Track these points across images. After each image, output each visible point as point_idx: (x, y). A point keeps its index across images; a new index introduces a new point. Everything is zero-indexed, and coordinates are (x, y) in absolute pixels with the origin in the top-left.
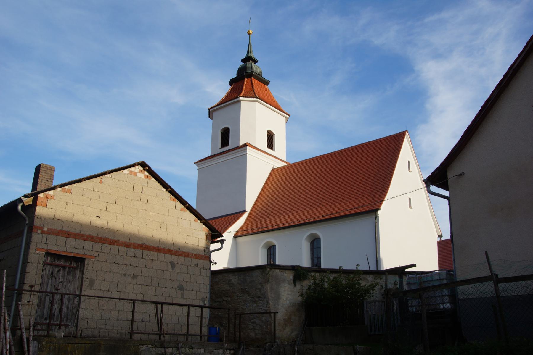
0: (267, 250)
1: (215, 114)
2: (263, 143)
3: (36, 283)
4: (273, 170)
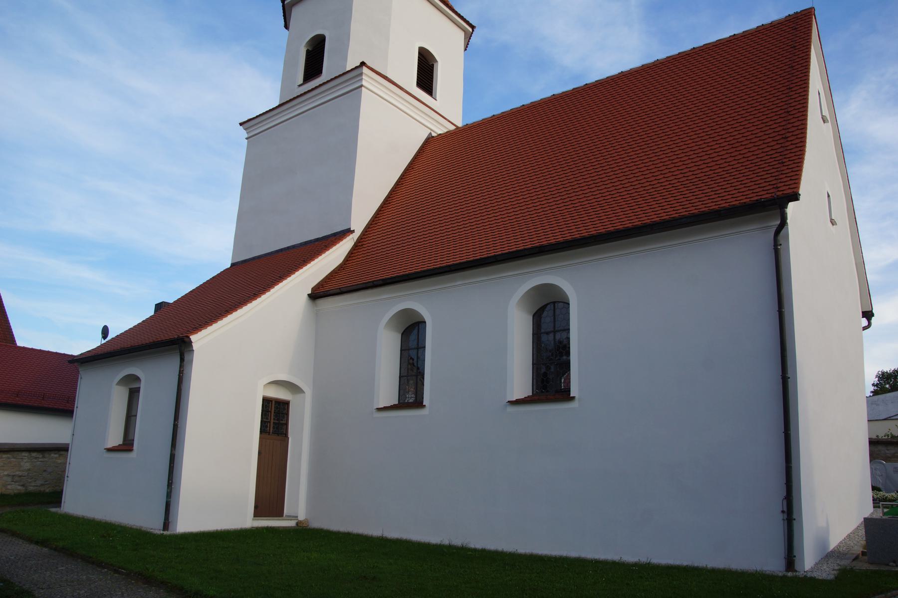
0: (400, 336)
2: (409, 75)
3: (416, 351)
4: (429, 140)
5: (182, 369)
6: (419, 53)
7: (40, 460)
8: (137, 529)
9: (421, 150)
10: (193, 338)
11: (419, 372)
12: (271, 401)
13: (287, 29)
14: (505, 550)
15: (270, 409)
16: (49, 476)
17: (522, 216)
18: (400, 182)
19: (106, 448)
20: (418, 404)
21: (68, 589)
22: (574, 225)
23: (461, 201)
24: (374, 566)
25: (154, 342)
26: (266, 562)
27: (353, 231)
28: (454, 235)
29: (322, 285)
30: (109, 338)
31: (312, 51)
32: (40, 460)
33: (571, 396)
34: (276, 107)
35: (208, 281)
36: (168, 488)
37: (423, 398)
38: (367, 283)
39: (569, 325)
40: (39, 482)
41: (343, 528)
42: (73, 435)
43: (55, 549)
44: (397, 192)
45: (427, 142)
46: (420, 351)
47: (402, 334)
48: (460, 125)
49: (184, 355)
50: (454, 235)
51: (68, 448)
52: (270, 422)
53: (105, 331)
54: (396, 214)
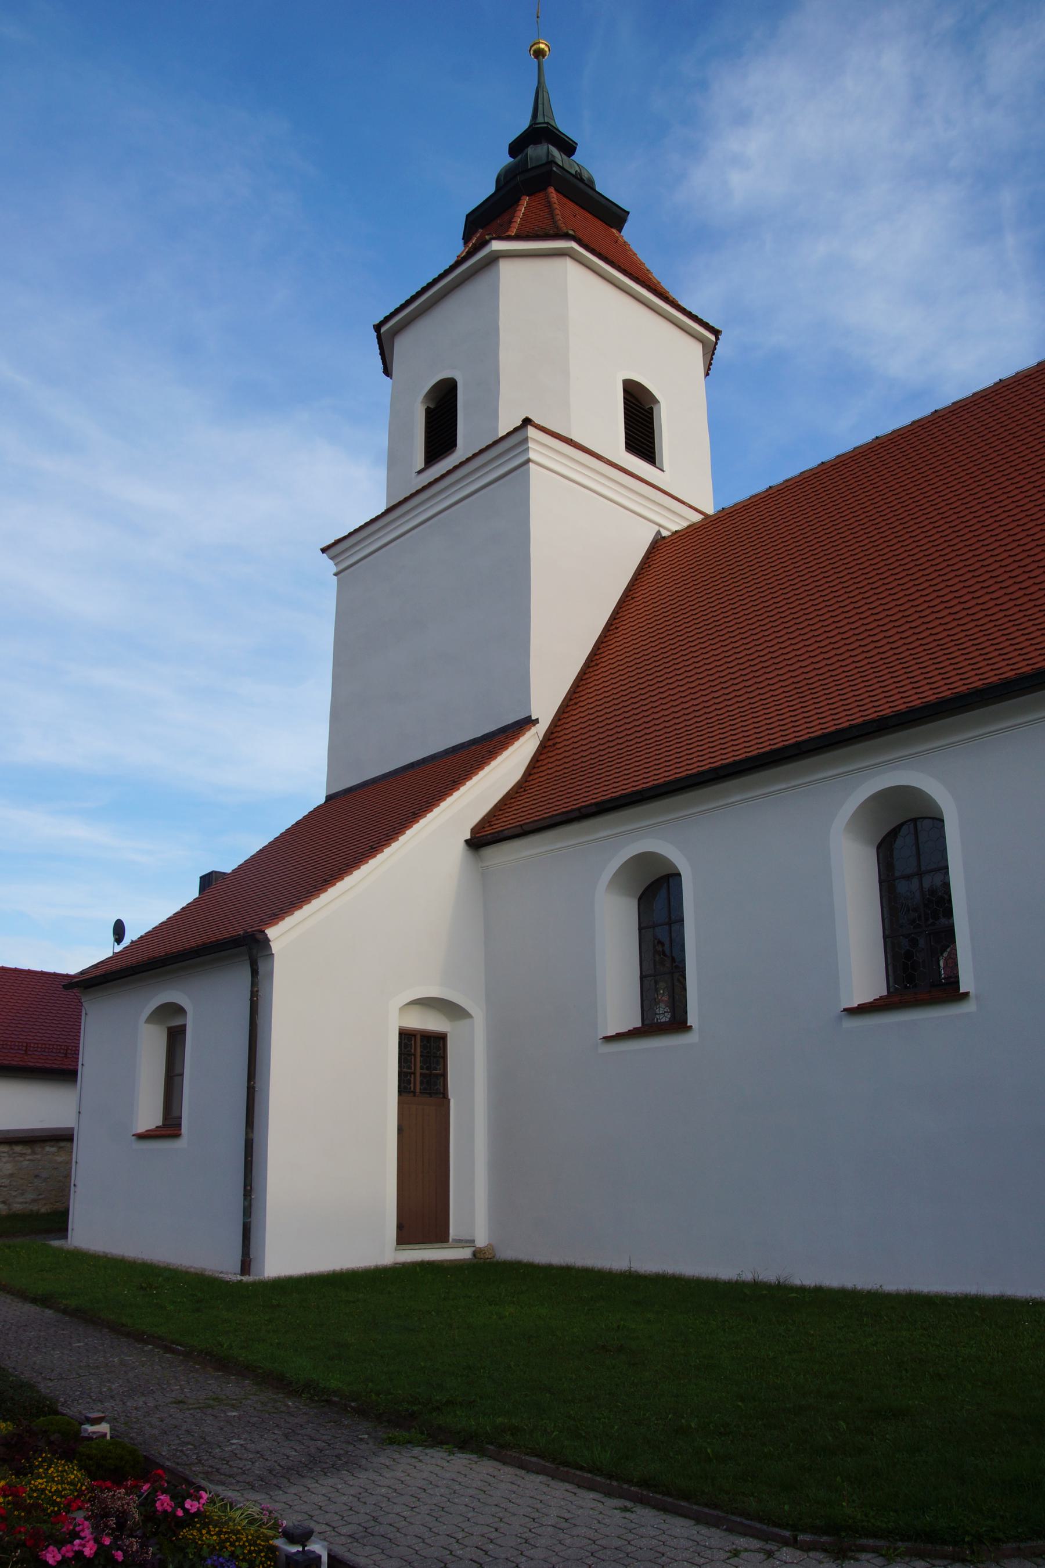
1: (402, 345)
4: (658, 544)
5: (256, 989)
6: (625, 391)
7: (28, 1157)
8: (196, 1274)
9: (645, 564)
10: (271, 932)
11: (677, 967)
12: (415, 1036)
13: (388, 376)
14: (859, 1287)
15: (413, 1051)
16: (44, 1184)
17: (817, 675)
18: (612, 625)
19: (134, 1133)
20: (679, 1024)
21: (92, 1381)
22: (936, 669)
23: (725, 649)
24: (618, 1327)
25: (204, 944)
26: (424, 1326)
27: (537, 721)
28: (719, 712)
29: (489, 822)
30: (126, 942)
31: (434, 409)
32: (28, 1157)
33: (961, 991)
34: (382, 513)
35: (288, 830)
36: (245, 1199)
37: (686, 1013)
38: (567, 812)
39: (947, 860)
40: (30, 1196)
41: (557, 1259)
42: (79, 1112)
43: (65, 1311)
44: (610, 643)
45: (654, 548)
46: (675, 927)
47: (640, 900)
48: (710, 510)
49: (257, 964)
50: (719, 712)
51: (73, 1135)
52: (414, 1073)
53: (119, 930)
54: (601, 686)
